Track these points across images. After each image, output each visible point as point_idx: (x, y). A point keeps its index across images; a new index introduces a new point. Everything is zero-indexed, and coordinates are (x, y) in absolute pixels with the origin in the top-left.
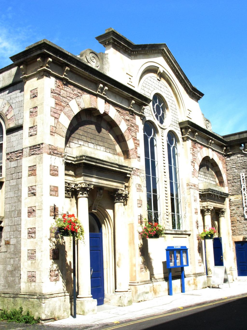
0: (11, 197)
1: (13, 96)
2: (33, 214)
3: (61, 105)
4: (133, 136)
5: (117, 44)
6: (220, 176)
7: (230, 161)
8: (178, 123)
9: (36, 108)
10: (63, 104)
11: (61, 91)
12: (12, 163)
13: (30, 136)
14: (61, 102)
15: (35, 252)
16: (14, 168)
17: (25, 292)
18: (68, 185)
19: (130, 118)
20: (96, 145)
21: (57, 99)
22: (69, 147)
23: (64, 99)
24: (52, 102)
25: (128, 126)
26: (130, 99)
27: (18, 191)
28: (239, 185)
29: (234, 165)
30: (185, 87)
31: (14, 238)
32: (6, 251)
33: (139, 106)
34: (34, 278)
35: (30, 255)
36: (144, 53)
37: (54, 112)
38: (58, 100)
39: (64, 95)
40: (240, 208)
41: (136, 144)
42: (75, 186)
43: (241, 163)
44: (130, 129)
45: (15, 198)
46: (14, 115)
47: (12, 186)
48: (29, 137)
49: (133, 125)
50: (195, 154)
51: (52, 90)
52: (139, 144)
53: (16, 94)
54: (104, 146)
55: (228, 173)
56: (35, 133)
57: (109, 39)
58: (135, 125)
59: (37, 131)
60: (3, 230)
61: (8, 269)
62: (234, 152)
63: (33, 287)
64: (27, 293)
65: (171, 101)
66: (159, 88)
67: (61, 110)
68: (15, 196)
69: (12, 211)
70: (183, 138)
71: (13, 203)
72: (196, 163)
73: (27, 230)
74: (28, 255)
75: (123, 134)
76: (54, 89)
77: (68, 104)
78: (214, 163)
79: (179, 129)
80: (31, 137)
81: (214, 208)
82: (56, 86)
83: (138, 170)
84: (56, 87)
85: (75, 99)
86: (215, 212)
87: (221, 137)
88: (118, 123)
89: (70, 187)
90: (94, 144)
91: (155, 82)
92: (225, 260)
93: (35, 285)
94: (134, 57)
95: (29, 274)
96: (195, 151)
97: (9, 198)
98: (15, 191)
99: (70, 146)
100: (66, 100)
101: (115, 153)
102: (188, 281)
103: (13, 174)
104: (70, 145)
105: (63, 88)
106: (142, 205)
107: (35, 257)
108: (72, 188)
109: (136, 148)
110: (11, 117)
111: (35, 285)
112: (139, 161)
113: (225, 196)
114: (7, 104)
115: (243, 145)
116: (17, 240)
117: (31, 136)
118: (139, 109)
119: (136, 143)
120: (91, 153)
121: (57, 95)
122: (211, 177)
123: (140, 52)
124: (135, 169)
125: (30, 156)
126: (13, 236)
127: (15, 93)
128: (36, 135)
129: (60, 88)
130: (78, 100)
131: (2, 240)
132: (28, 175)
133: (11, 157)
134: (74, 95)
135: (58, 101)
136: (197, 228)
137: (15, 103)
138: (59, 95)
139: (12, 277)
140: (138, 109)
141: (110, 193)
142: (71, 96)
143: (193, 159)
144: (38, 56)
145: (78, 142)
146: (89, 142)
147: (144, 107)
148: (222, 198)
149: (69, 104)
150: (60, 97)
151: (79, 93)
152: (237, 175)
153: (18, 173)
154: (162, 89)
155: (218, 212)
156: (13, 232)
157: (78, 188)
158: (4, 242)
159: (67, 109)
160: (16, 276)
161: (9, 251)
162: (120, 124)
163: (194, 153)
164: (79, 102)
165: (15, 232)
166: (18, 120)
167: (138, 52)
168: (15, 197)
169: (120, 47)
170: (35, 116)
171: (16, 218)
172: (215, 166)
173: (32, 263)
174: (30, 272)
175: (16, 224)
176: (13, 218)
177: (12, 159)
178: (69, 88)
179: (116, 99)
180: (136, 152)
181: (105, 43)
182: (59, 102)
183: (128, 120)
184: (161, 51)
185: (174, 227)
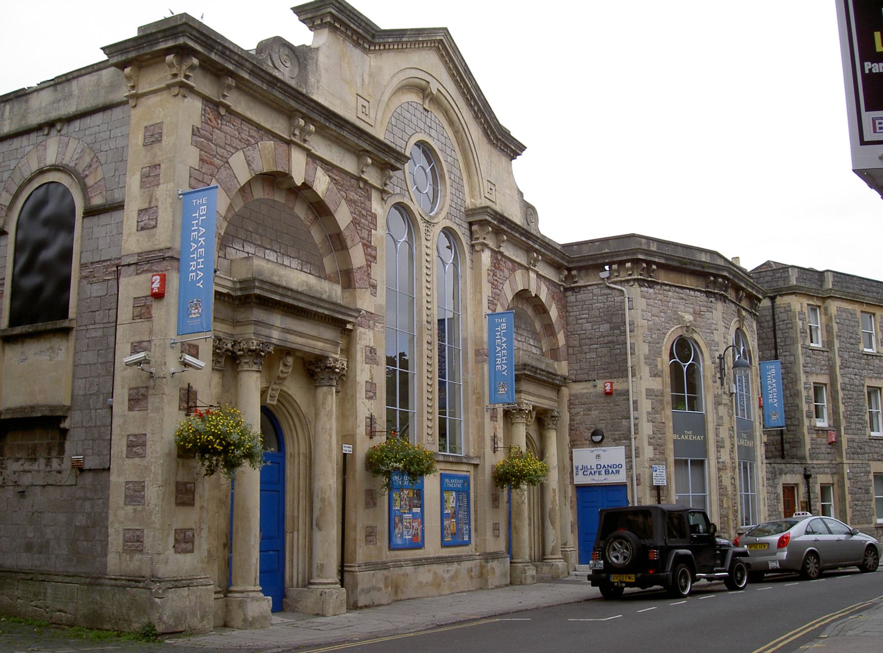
0: (90, 364)
1: (102, 135)
2: (143, 403)
3: (212, 164)
4: (361, 238)
5: (341, 26)
6: (552, 335)
7: (576, 304)
8: (463, 211)
9: (157, 167)
10: (216, 161)
11: (213, 131)
12: (95, 287)
13: (139, 229)
14: (211, 157)
15: (144, 487)
16: (99, 299)
17: (119, 574)
18: (218, 342)
19: (360, 196)
20: (282, 255)
21: (203, 148)
22: (223, 256)
23: (220, 151)
24: (192, 156)
25: (354, 215)
26: (362, 153)
27: (106, 350)
28: (592, 360)
29: (584, 312)
30: (484, 127)
31: (93, 454)
32: (75, 483)
33: (379, 171)
34: (140, 543)
35: (132, 493)
36: (398, 48)
37: (197, 180)
38: (206, 152)
39: (218, 141)
40: (593, 412)
41: (369, 257)
42: (232, 346)
43: (601, 310)
44: (357, 222)
45: (99, 366)
46: (104, 178)
47: (93, 338)
48: (138, 230)
49: (364, 212)
50: (499, 284)
51: (195, 129)
52: (375, 258)
53: (110, 131)
54: (298, 259)
55: (569, 330)
56: (153, 223)
57: (322, 15)
58: (369, 213)
59: (156, 220)
60: (68, 435)
61: (77, 524)
62: (587, 284)
63: (135, 564)
64: (121, 576)
65: (449, 159)
66: (427, 130)
67: (212, 175)
68: (100, 361)
69: (90, 394)
70: (473, 246)
71: (93, 377)
72: (499, 305)
73: (125, 438)
74: (125, 492)
75: (342, 232)
76: (200, 127)
77: (227, 162)
78: (541, 305)
79: (466, 225)
80: (143, 232)
81: (534, 407)
82: (203, 120)
83: (370, 315)
84: (202, 122)
85: (243, 151)
86: (536, 417)
87: (559, 248)
88: (332, 207)
89: (223, 347)
90: (276, 252)
91: (418, 114)
92: (552, 527)
93: (142, 559)
94: (376, 56)
95: (127, 535)
96: (498, 275)
97: (85, 365)
98: (101, 350)
99: (225, 255)
100: (223, 153)
101: (321, 275)
102: (468, 568)
103: (95, 311)
104: (227, 254)
105: (218, 124)
106: (375, 394)
107: (143, 497)
108: (228, 350)
109: (370, 266)
110: (96, 183)
111: (141, 560)
112: (374, 294)
113: (18, 330)
114: (88, 151)
115: (607, 268)
116: (101, 461)
117: (143, 229)
118: (380, 177)
119: (370, 255)
120: (273, 274)
121: (206, 142)
122: (530, 336)
123: (389, 45)
124: (365, 313)
125: (139, 274)
126: (91, 450)
127: (108, 128)
128: (155, 229)
129: (212, 124)
130: (251, 152)
131: (64, 459)
132: (131, 316)
133: (93, 273)
134: (240, 141)
135: (206, 154)
136: (494, 452)
137: (106, 151)
138: (211, 141)
139: (87, 541)
140: (377, 177)
141: (307, 364)
142: (236, 143)
143: (493, 296)
144: (168, 51)
145: (243, 247)
146: (267, 249)
147: (392, 173)
148: (554, 383)
149: (229, 161)
150: (212, 145)
151: (252, 137)
152: (590, 336)
153: (109, 310)
154: (433, 133)
155: (543, 418)
156: (91, 442)
157: (240, 350)
158: (70, 463)
159: (223, 174)
160: (97, 538)
161: (80, 483)
162: (335, 211)
163: (496, 280)
164: (250, 158)
165: (97, 441)
166: (113, 190)
167: (384, 46)
168: (100, 363)
169: (346, 33)
170: (155, 185)
171: (100, 410)
172: (542, 312)
173: (135, 510)
174: (131, 532)
175: (98, 423)
176: (92, 411)
177: (94, 277)
178: (231, 125)
179: (331, 152)
180: (369, 274)
181: (314, 22)
182: (209, 156)
183: (355, 202)
184: (436, 45)
185: (443, 447)
